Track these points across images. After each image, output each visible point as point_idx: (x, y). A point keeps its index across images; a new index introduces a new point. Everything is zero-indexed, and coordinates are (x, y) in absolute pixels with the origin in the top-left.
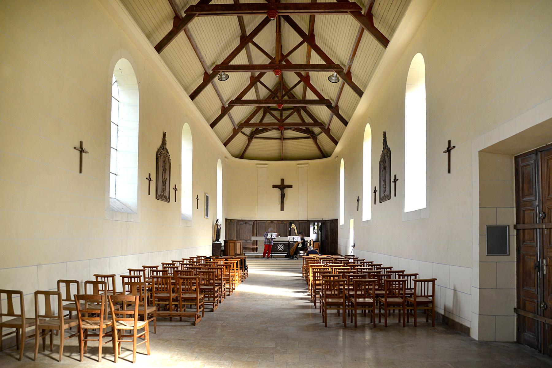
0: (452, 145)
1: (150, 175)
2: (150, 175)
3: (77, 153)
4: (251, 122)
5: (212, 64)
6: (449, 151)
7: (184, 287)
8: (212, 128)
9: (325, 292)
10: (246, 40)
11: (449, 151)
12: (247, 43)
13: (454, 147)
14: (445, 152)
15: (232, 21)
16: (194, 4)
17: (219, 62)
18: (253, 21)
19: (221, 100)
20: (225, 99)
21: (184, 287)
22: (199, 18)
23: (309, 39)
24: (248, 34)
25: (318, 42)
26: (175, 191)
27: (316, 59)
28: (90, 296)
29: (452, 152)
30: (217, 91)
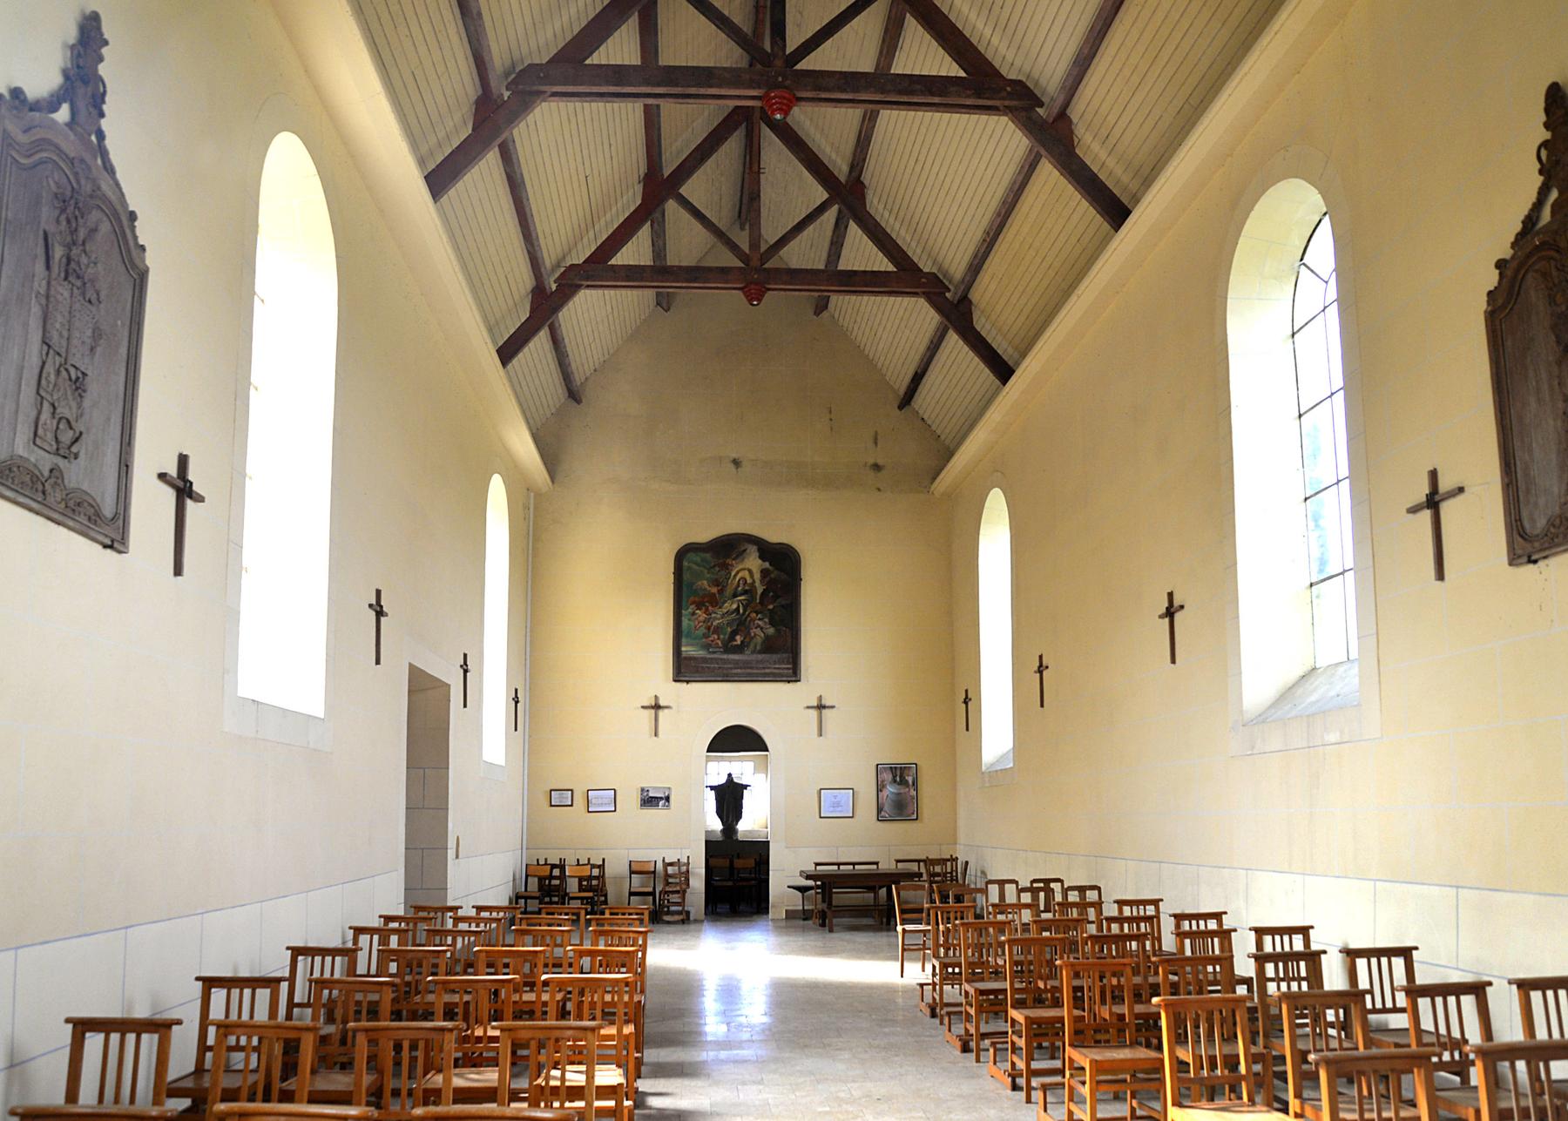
0: (1176, 603)
1: (378, 593)
2: (378, 593)
3: (169, 495)
4: (618, 260)
5: (558, 265)
6: (1170, 613)
7: (1117, 1009)
8: (504, 364)
9: (395, 931)
10: (659, 187)
11: (1170, 613)
12: (663, 201)
13: (1182, 607)
14: (1161, 617)
15: (625, 117)
16: (576, 262)
17: (579, 258)
18: (687, 122)
19: (480, 63)
20: (499, 57)
21: (1117, 1009)
22: (588, 291)
23: (848, 195)
24: (667, 172)
25: (876, 205)
26: (466, 671)
27: (861, 254)
28: (1330, 1007)
29: (1178, 616)
30: (515, 185)
